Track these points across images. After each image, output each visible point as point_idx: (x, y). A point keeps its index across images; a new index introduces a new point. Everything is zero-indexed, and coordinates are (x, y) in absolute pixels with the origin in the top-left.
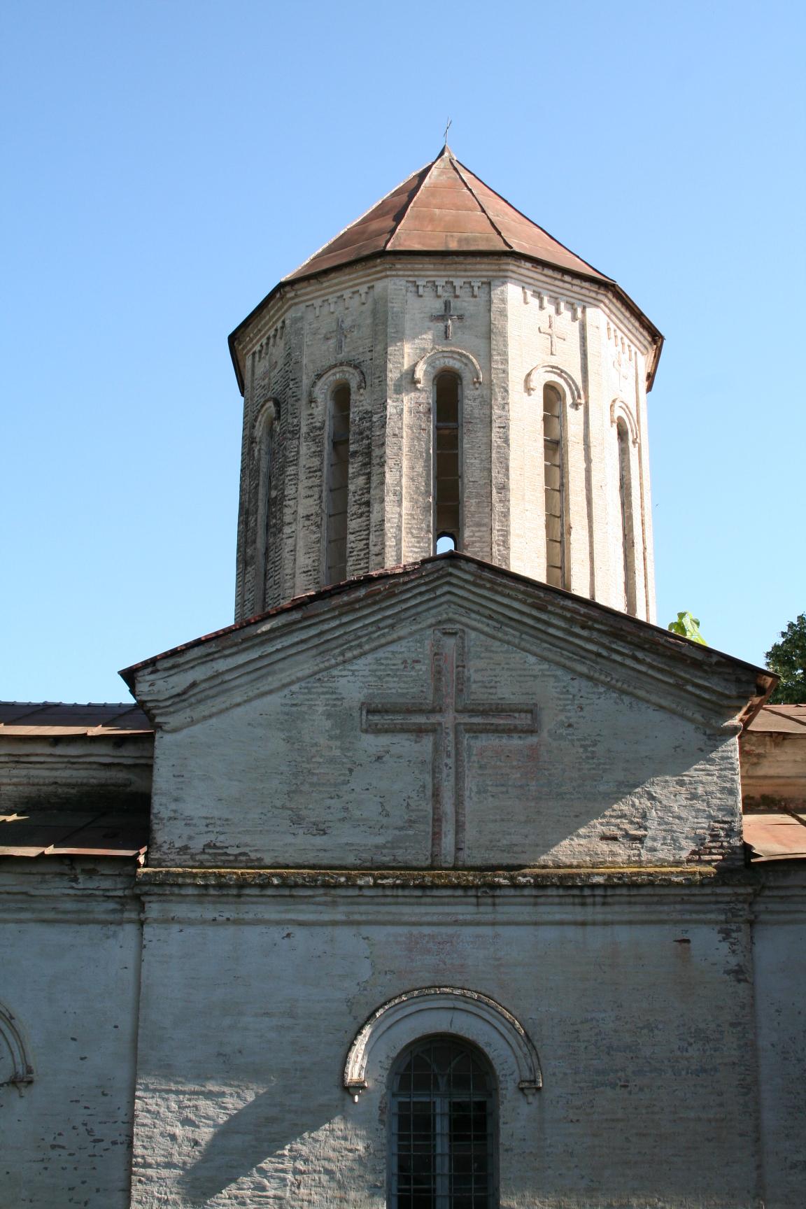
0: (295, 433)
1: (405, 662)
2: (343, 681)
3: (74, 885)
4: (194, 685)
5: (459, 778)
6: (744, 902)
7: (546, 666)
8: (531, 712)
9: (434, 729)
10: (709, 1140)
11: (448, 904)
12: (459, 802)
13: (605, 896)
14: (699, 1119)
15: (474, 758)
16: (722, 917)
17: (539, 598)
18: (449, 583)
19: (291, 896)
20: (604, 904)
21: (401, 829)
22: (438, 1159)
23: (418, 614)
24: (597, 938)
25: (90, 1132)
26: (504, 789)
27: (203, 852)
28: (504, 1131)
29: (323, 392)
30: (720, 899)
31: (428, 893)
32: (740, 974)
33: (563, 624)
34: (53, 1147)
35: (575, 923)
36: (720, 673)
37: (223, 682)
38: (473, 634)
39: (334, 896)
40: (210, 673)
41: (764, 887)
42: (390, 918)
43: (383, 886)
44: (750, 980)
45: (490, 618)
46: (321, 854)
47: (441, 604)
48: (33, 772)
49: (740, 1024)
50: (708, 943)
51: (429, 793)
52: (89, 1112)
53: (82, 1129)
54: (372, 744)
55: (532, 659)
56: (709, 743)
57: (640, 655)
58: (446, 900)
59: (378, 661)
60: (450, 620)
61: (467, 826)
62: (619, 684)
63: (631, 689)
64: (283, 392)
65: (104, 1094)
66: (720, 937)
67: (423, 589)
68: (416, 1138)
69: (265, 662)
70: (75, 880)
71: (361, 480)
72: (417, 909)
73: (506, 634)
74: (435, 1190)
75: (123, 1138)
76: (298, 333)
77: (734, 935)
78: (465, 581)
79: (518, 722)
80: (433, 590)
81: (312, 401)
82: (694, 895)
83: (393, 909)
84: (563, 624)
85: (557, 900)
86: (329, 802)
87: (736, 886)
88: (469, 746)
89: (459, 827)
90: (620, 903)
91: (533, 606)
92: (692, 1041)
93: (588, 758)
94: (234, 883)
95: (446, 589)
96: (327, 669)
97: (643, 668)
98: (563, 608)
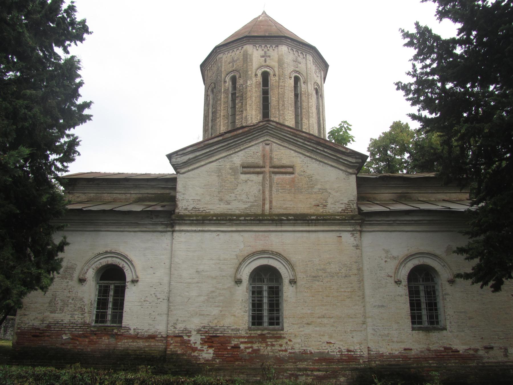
0: (220, 91)
1: (254, 152)
2: (235, 158)
12: (271, 195)
14: (345, 292)
18: (268, 129)
21: (253, 202)
25: (156, 296)
28: (285, 295)
29: (228, 79)
32: (357, 247)
34: (144, 301)
38: (274, 144)
43: (247, 220)
49: (357, 262)
51: (261, 192)
53: (154, 295)
54: (243, 177)
60: (267, 140)
61: (273, 202)
64: (216, 80)
68: (258, 297)
70: (152, 218)
71: (240, 104)
75: (166, 298)
76: (221, 62)
80: (262, 131)
81: (225, 82)
89: (271, 202)
94: (203, 220)
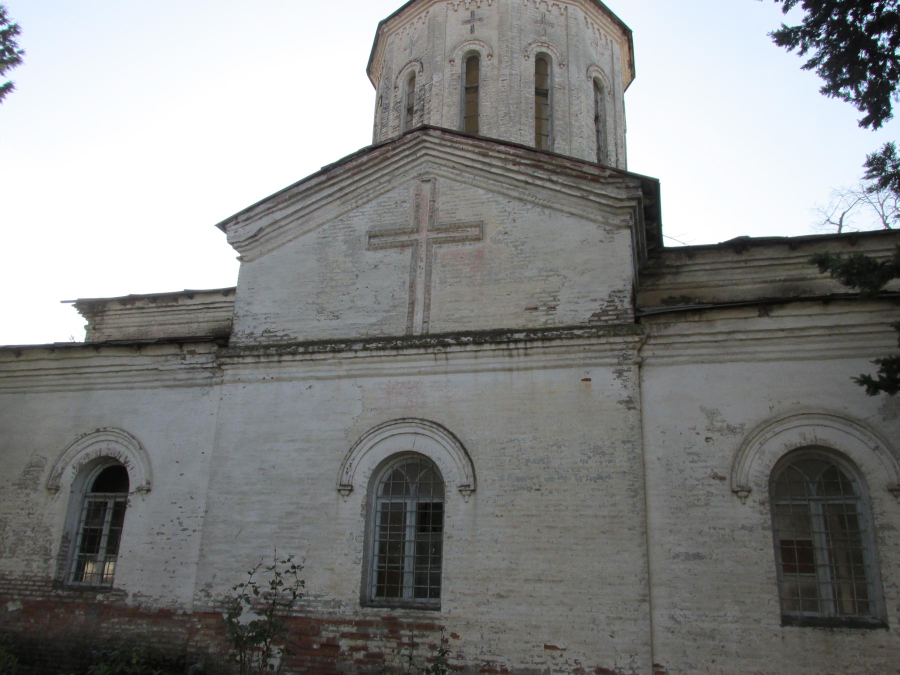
3: (184, 362)
4: (261, 230)
5: (429, 274)
6: (633, 349)
7: (490, 195)
8: (479, 226)
9: (414, 244)
10: (604, 533)
11: (415, 360)
12: (428, 290)
13: (526, 349)
14: (596, 516)
15: (438, 261)
16: (616, 361)
17: (482, 147)
19: (312, 360)
20: (526, 355)
21: (387, 312)
22: (407, 545)
23: (406, 171)
24: (520, 380)
25: (180, 524)
26: (458, 280)
27: (262, 336)
30: (614, 347)
31: (401, 352)
33: (500, 164)
34: (158, 534)
35: (504, 370)
36: (612, 183)
37: (281, 227)
38: (442, 180)
39: (340, 359)
40: (271, 221)
41: (649, 337)
42: (375, 372)
44: (638, 407)
45: (454, 168)
46: (335, 332)
47: (421, 164)
48: (217, 314)
49: (629, 442)
50: (607, 383)
51: (407, 286)
52: (181, 510)
53: (176, 521)
55: (481, 192)
56: (607, 236)
57: (554, 178)
58: (413, 357)
59: (379, 204)
60: (427, 173)
62: (541, 202)
63: (550, 204)
65: (192, 498)
66: (615, 376)
67: (407, 153)
69: (306, 211)
70: (184, 359)
72: (395, 365)
73: (463, 177)
74: (403, 568)
77: (625, 374)
78: (435, 143)
79: (469, 234)
82: (593, 345)
83: (379, 366)
84: (500, 164)
85: (491, 353)
86: (342, 297)
87: (624, 335)
88: (436, 253)
89: (427, 307)
90: (538, 354)
91: (479, 154)
92: (591, 454)
93: (518, 254)
95: (423, 152)
96: (347, 212)
97: (558, 188)
98: (499, 152)
